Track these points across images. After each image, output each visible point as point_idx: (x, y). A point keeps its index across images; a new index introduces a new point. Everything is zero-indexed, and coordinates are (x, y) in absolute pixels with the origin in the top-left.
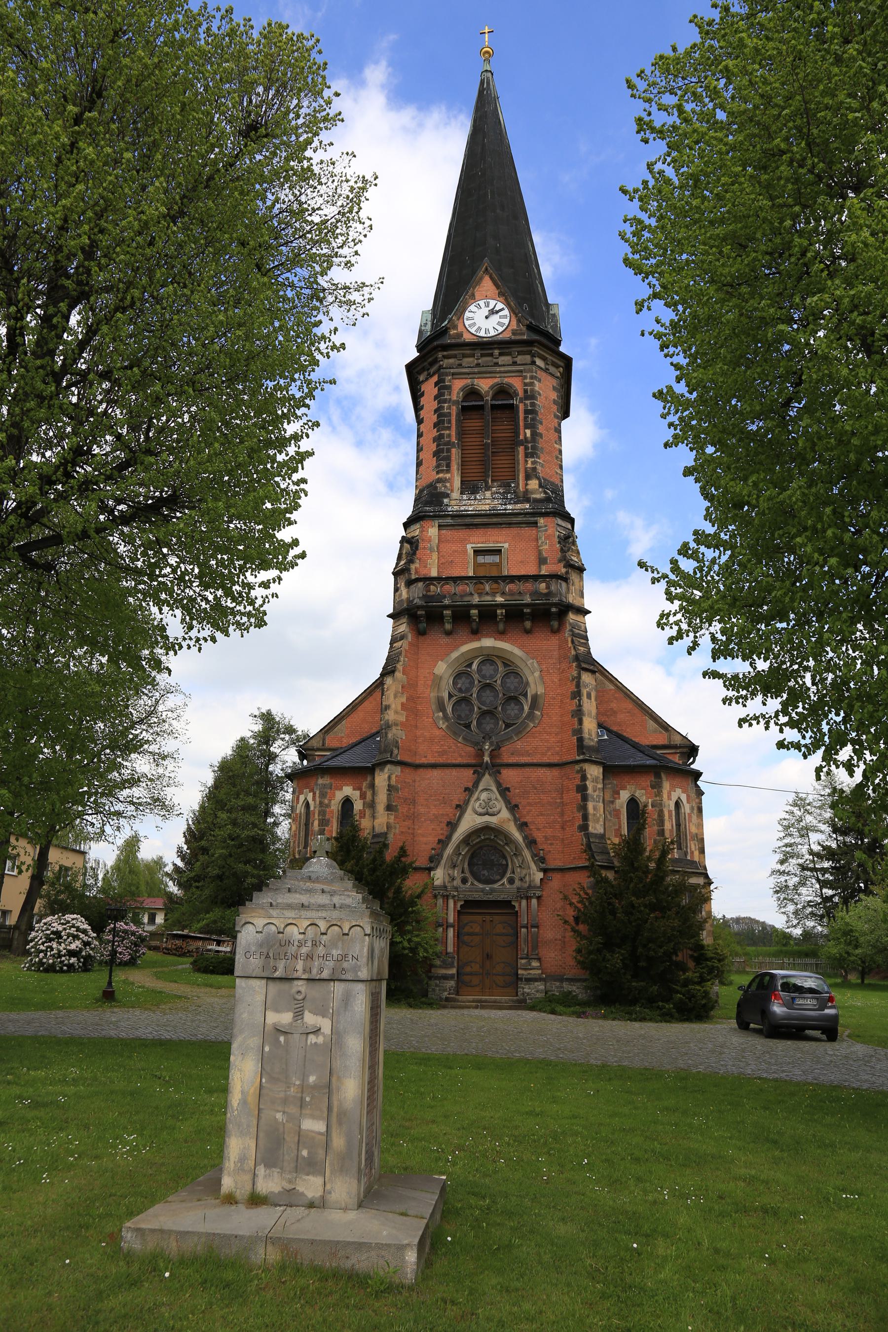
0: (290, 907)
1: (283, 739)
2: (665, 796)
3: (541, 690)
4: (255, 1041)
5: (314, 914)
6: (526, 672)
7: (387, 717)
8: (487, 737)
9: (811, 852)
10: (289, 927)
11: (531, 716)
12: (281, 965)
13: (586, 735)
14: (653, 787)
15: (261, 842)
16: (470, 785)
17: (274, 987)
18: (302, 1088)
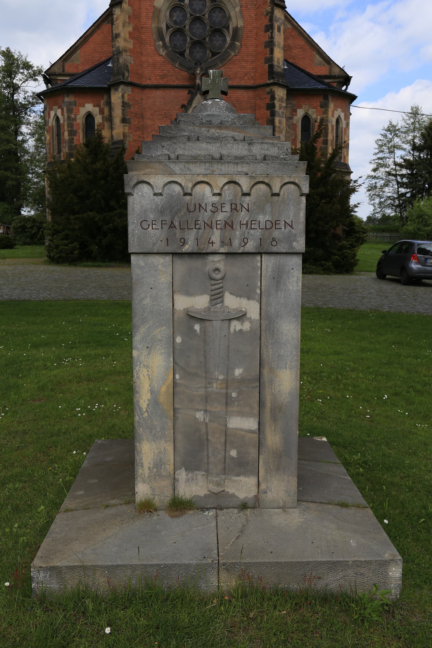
0: (195, 159)
1: (22, 73)
2: (330, 114)
3: (240, 24)
4: (162, 332)
5: (231, 169)
6: (230, 7)
7: (117, 44)
8: (198, 63)
9: (396, 164)
10: (199, 188)
11: (232, 46)
12: (191, 237)
13: (275, 63)
14: (322, 107)
15: (16, 154)
16: (185, 103)
17: (182, 266)
18: (227, 383)
